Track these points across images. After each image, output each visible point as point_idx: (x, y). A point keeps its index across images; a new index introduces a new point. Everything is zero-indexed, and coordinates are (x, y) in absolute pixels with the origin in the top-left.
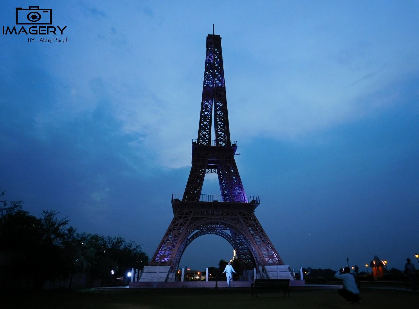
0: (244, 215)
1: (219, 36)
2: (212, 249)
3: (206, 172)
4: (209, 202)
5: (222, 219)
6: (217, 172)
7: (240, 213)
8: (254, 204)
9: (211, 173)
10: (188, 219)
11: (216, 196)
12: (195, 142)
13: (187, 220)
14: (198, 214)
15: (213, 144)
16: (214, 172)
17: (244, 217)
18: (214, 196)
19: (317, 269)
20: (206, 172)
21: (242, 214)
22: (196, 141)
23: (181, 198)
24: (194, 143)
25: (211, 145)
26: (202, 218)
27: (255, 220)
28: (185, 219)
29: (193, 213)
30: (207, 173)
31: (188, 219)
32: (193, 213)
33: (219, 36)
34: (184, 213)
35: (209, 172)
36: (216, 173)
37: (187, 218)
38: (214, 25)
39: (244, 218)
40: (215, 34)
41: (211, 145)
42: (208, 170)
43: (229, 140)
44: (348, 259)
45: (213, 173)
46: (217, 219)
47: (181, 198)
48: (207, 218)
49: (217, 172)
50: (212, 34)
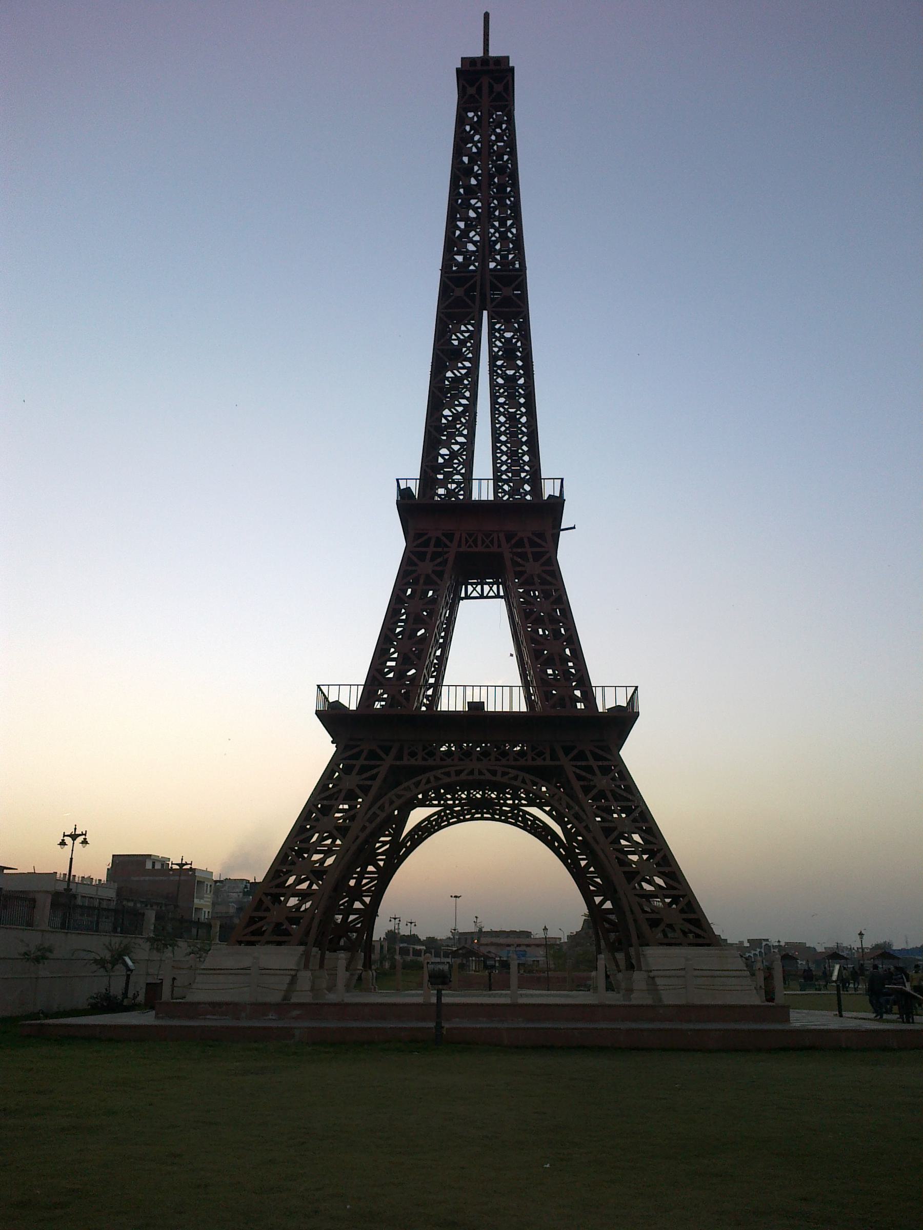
0: (581, 756)
1: (507, 59)
2: (479, 870)
3: (463, 595)
4: (456, 713)
5: (367, 824)
6: (502, 594)
7: (567, 750)
8: (623, 719)
9: (482, 596)
10: (377, 774)
11: (484, 690)
12: (408, 489)
13: (373, 778)
14: (413, 754)
15: (483, 491)
16: (491, 594)
17: (579, 763)
18: (469, 690)
19: (820, 949)
20: (463, 595)
21: (571, 756)
22: (414, 486)
23: (351, 700)
24: (404, 495)
25: (475, 496)
26: (425, 770)
27: (624, 774)
28: (364, 776)
29: (394, 751)
30: (467, 597)
31: (377, 774)
32: (394, 751)
33: (507, 59)
34: (362, 751)
35: (475, 594)
36: (497, 596)
37: (374, 772)
38: (487, 16)
39: (576, 766)
40: (492, 53)
41: (475, 496)
42: (470, 588)
43: (536, 478)
44: (861, 934)
45: (487, 597)
46: (480, 773)
47: (351, 700)
48: (443, 770)
49: (502, 594)
50: (480, 53)
